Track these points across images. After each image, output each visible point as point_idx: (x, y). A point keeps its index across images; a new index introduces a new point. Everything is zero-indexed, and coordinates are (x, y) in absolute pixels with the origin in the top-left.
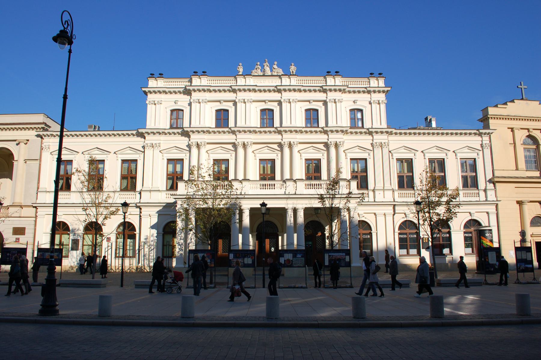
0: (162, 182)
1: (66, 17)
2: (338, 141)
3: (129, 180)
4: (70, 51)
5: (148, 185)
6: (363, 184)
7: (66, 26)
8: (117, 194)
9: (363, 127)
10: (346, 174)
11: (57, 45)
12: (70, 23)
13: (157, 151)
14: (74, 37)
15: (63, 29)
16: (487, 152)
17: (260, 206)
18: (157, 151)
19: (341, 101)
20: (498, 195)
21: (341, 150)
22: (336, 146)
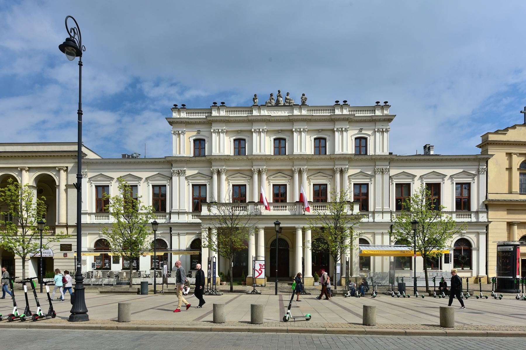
0: (188, 206)
1: (71, 24)
2: (343, 167)
3: (160, 203)
4: (80, 64)
5: (176, 208)
6: (364, 207)
7: (72, 34)
8: (454, 215)
9: (366, 154)
10: (350, 196)
11: (64, 55)
12: (77, 30)
13: (183, 178)
14: (83, 48)
15: (69, 37)
16: (483, 177)
17: (274, 225)
18: (183, 178)
19: (346, 130)
20: (489, 217)
21: (346, 176)
22: (342, 172)
